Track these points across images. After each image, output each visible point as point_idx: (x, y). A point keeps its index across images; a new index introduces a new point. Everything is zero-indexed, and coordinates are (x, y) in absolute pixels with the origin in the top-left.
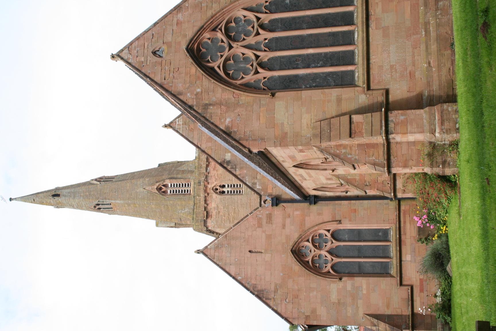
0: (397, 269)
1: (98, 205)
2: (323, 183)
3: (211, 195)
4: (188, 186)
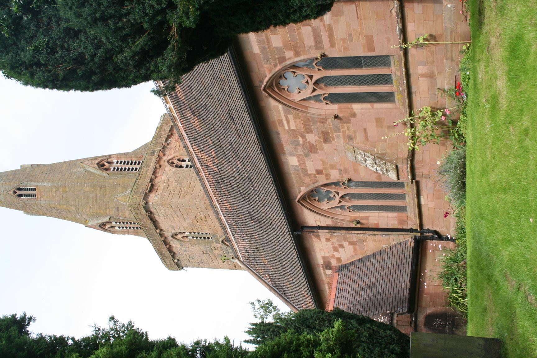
1: (20, 189)
3: (164, 168)
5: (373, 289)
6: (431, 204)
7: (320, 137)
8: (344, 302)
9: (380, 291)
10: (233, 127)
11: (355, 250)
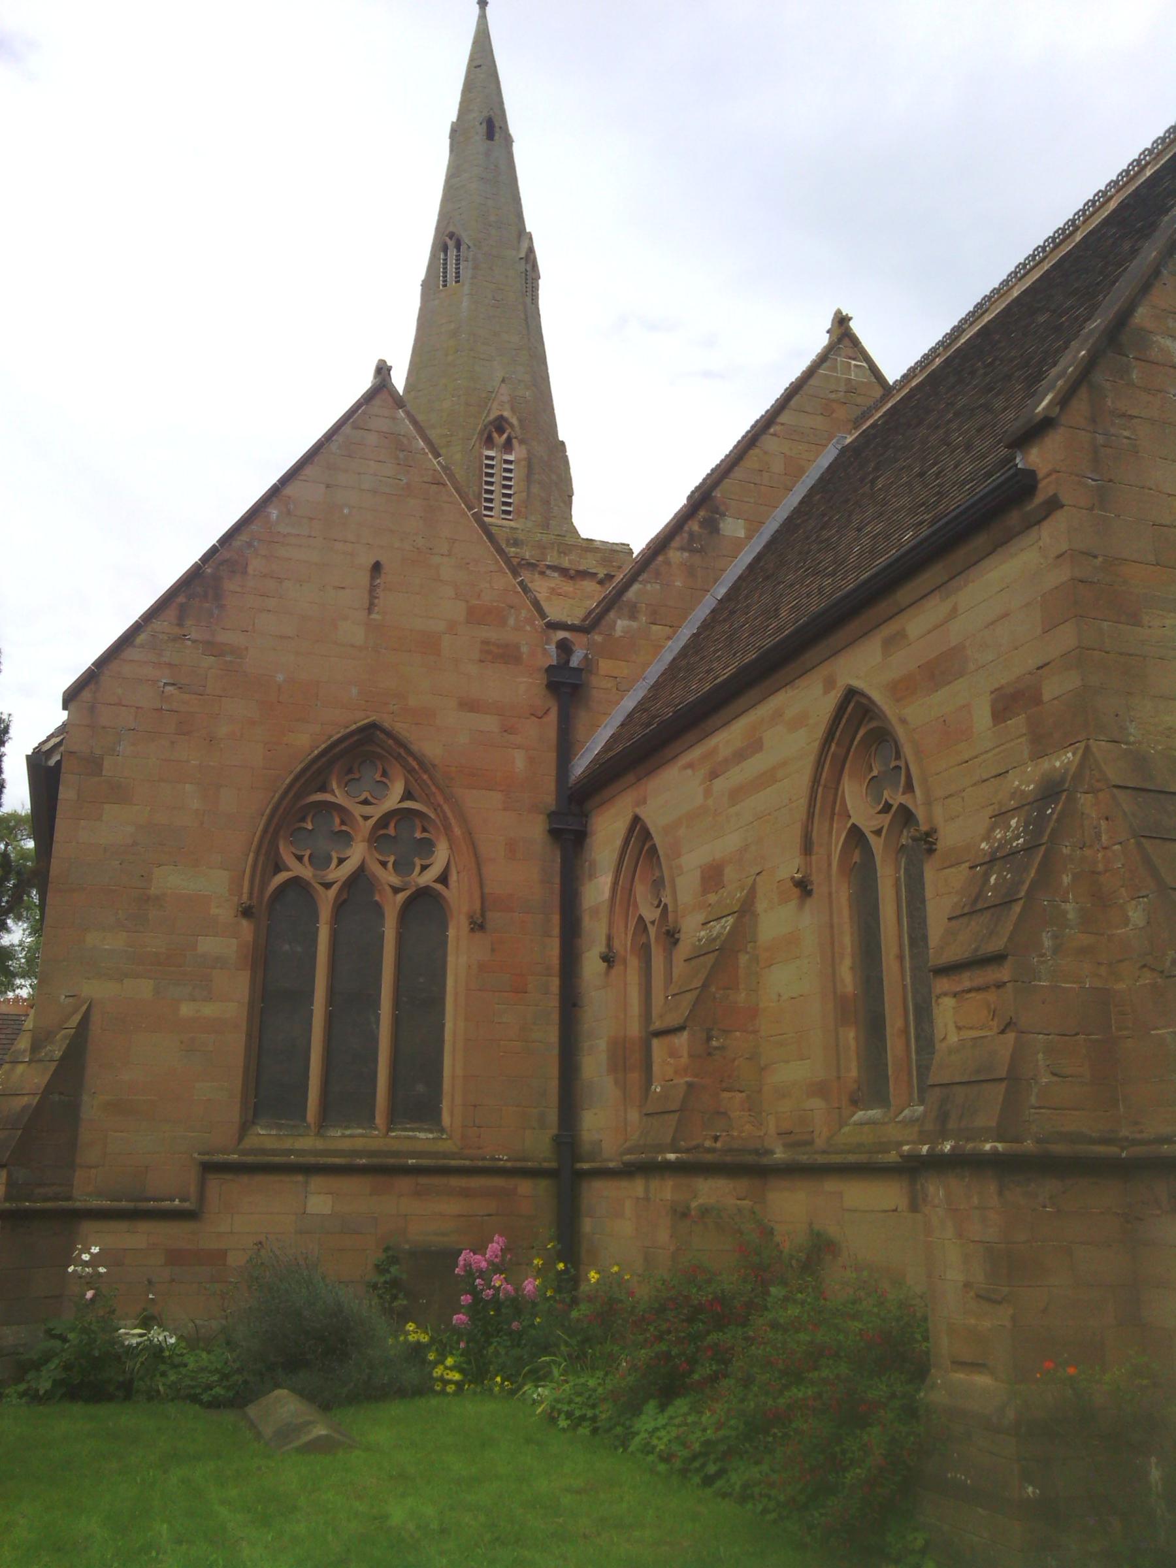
0: (274, 1152)
1: (458, 246)
2: (679, 856)
4: (505, 512)
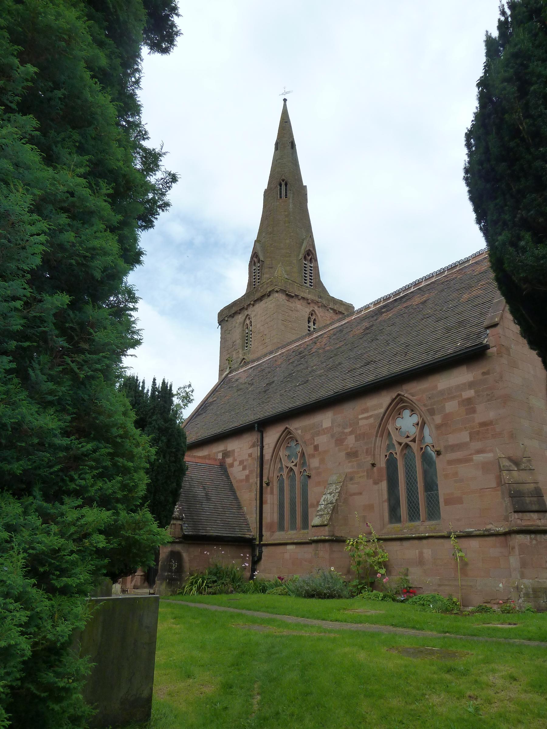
5: (205, 499)
6: (287, 556)
7: (351, 448)
8: (193, 471)
9: (203, 506)
10: (358, 366)
11: (241, 481)
